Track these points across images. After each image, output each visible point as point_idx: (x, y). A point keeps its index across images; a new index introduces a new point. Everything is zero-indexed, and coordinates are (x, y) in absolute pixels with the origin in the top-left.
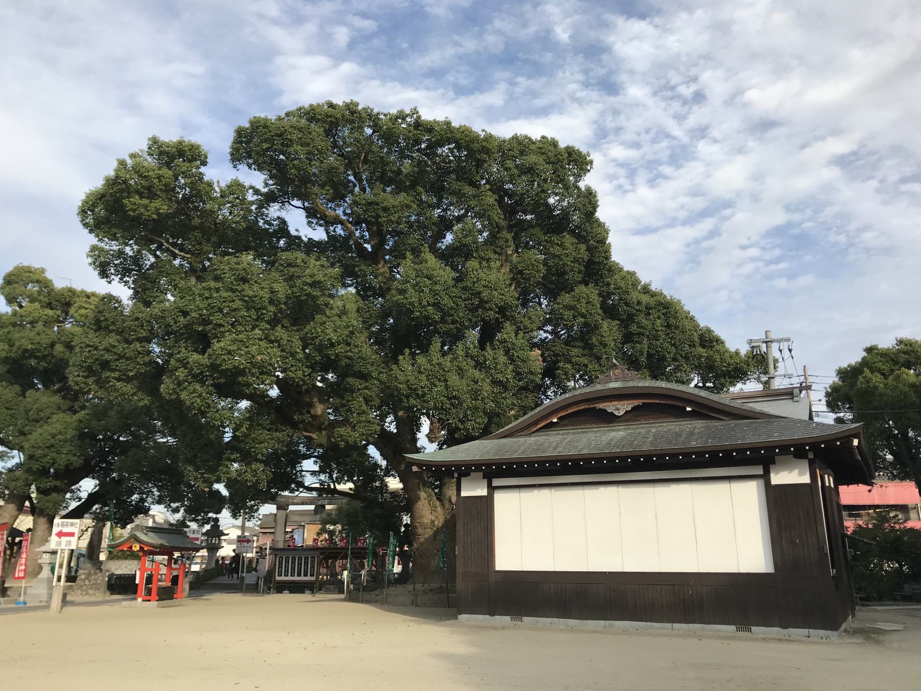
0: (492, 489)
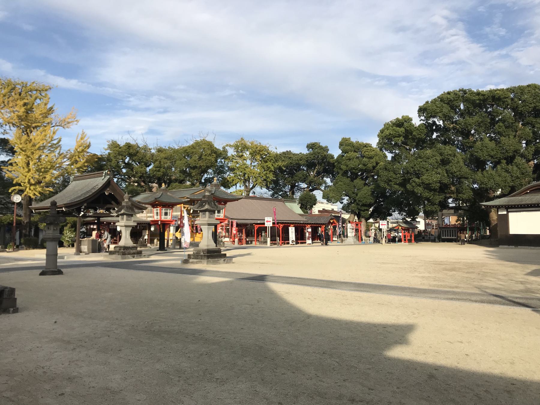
0: (508, 212)
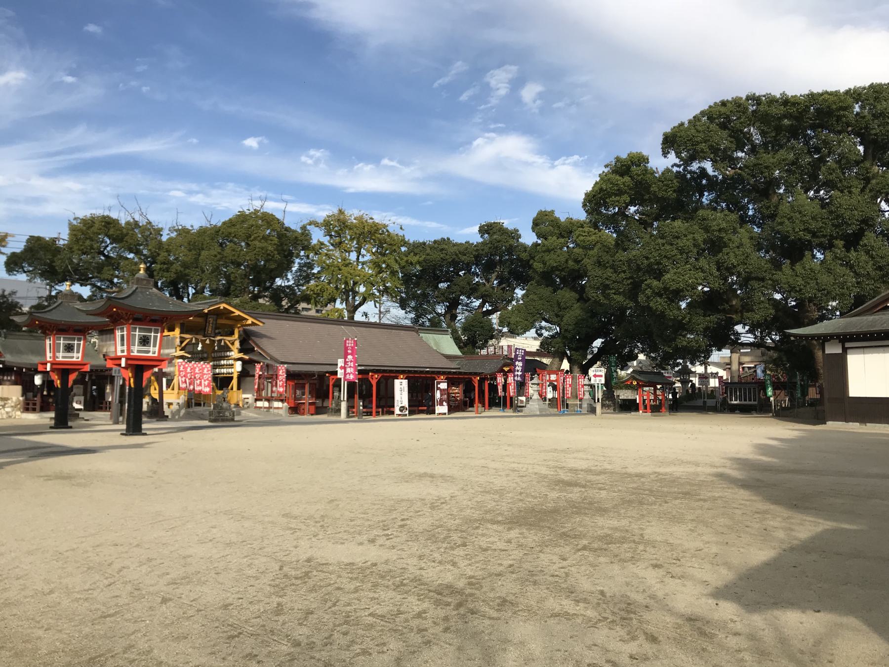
0: (845, 350)
